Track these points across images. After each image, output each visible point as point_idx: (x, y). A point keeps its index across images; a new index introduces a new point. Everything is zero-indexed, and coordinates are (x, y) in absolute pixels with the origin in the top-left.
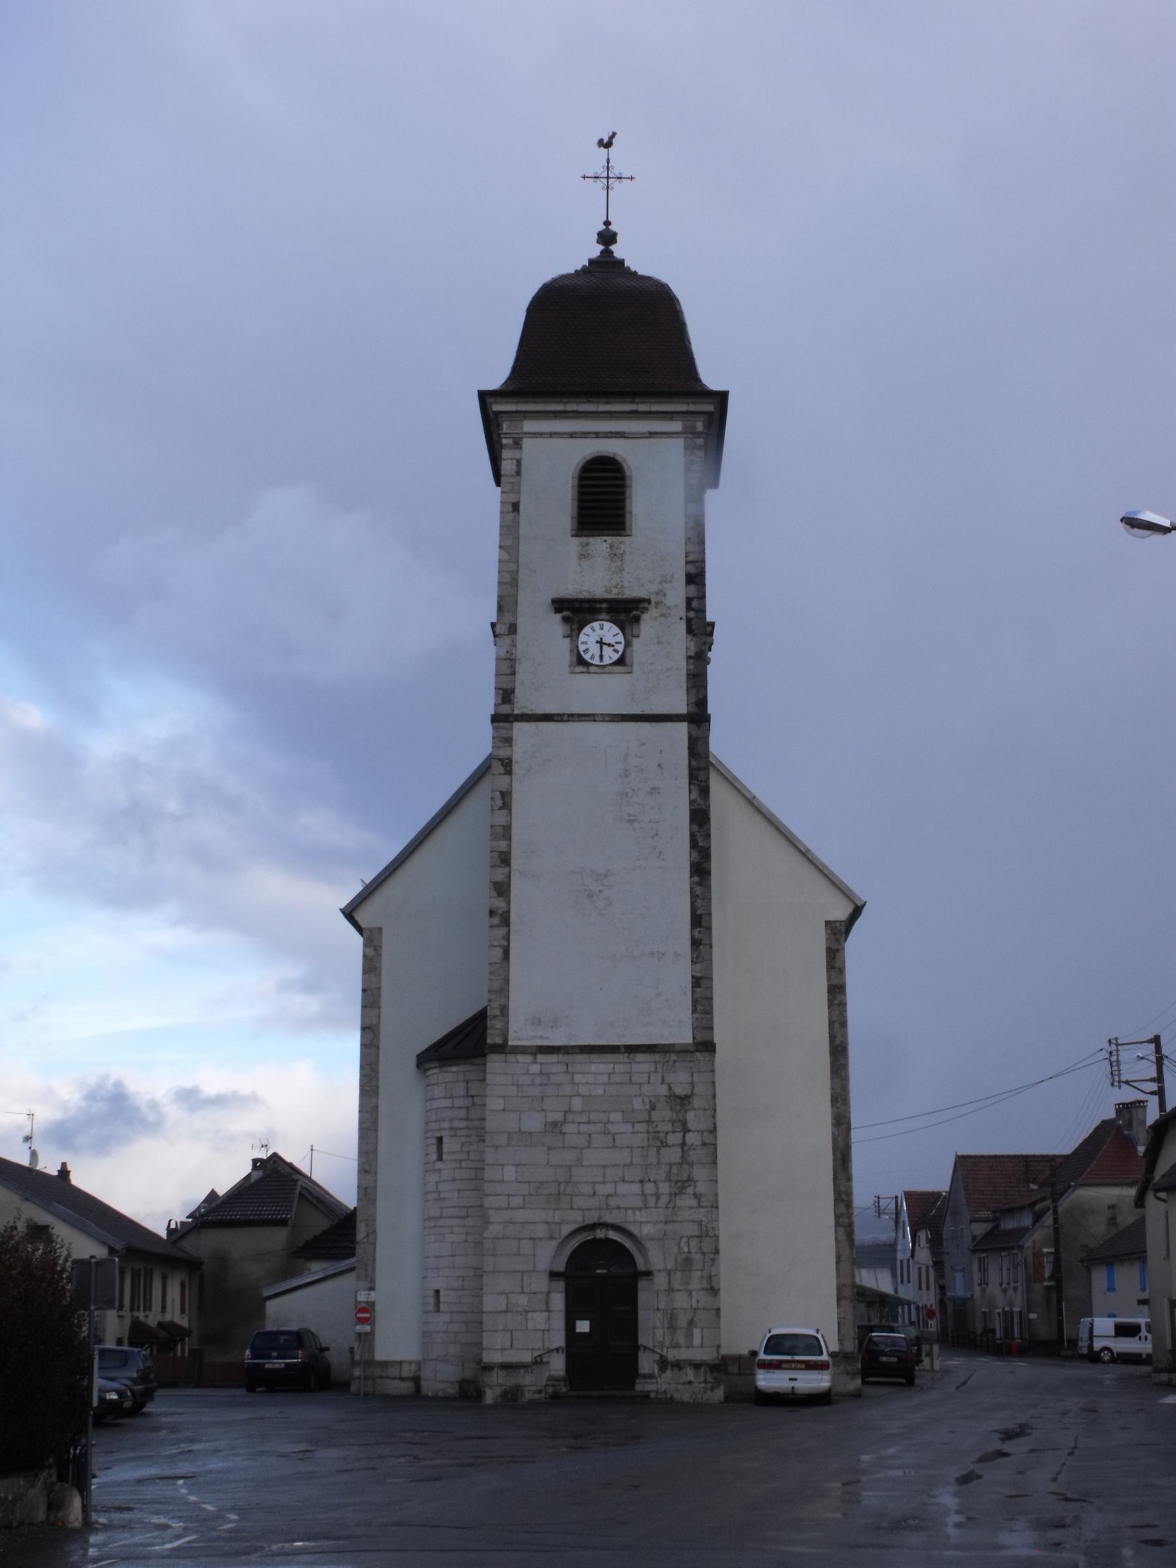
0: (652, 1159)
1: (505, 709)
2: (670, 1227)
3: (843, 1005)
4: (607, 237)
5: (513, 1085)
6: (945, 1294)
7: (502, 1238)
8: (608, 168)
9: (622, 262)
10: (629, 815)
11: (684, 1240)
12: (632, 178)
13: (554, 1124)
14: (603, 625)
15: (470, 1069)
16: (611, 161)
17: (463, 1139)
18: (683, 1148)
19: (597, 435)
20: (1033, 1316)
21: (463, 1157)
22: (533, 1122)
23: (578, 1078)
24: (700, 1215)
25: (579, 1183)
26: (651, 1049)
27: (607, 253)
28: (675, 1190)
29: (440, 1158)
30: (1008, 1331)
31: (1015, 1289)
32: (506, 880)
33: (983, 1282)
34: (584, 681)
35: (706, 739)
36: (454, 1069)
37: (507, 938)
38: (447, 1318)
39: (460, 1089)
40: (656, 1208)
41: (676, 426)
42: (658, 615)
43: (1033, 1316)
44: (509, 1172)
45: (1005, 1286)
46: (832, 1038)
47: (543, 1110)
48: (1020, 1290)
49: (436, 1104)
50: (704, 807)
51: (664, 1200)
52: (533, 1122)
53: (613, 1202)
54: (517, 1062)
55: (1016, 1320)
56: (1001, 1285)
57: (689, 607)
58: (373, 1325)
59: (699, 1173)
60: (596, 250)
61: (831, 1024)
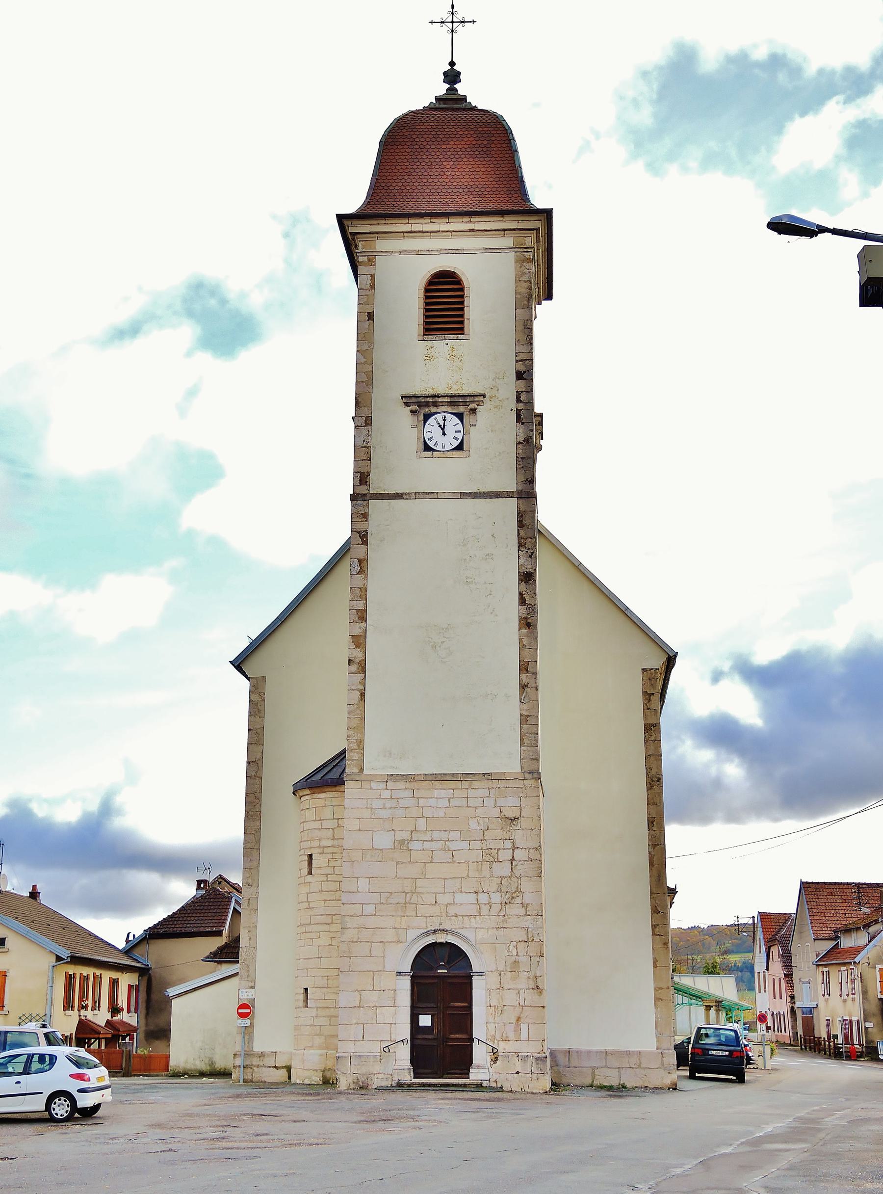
0: (486, 873)
1: (362, 489)
2: (501, 932)
3: (658, 742)
4: (452, 76)
5: (367, 808)
6: (794, 1003)
7: (357, 942)
8: (453, 13)
9: (464, 98)
10: (467, 578)
11: (514, 944)
12: (474, 22)
13: (402, 842)
14: (445, 417)
15: (336, 795)
16: (455, 7)
17: (330, 856)
18: (512, 863)
19: (440, 252)
20: (868, 1025)
21: (330, 871)
22: (384, 840)
23: (422, 802)
24: (528, 922)
25: (423, 893)
26: (486, 776)
27: (452, 90)
28: (505, 900)
29: (310, 873)
30: (847, 1038)
31: (853, 1000)
32: (363, 634)
33: (826, 994)
34: (429, 463)
35: (534, 512)
36: (322, 795)
37: (363, 682)
38: (314, 1013)
39: (327, 813)
40: (489, 916)
41: (508, 242)
42: (492, 407)
43: (868, 1025)
44: (363, 884)
45: (844, 997)
46: (648, 769)
47: (393, 830)
48: (857, 1000)
49: (307, 826)
50: (531, 570)
51: (496, 909)
52: (384, 840)
53: (452, 910)
54: (371, 789)
55: (855, 1028)
56: (841, 996)
57: (518, 400)
58: (252, 1019)
59: (526, 886)
60: (442, 89)
61: (648, 757)
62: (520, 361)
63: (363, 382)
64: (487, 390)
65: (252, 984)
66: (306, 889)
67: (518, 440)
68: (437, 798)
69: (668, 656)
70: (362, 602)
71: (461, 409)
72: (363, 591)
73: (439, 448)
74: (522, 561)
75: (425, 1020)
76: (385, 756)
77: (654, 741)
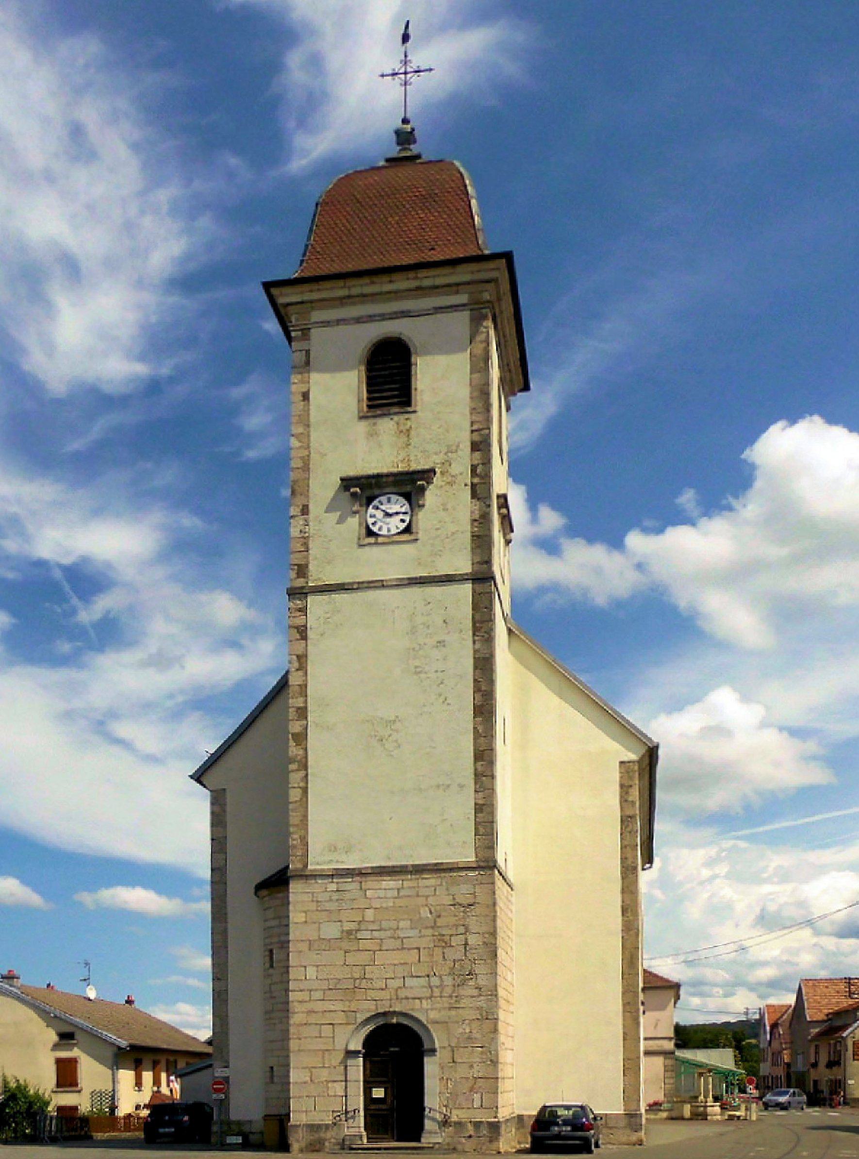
13: (349, 932)
18: (465, 948)
19: (383, 317)
24: (482, 1002)
29: (272, 966)
34: (375, 553)
44: (311, 972)
53: (402, 993)
59: (481, 969)
62: (476, 431)
63: (298, 468)
64: (439, 466)
65: (226, 1064)
66: (269, 981)
67: (473, 518)
68: (385, 889)
69: (647, 748)
70: (302, 699)
71: (408, 488)
72: (303, 687)
73: (384, 532)
74: (478, 646)
75: (378, 1093)
76: (330, 851)
77: (630, 832)
